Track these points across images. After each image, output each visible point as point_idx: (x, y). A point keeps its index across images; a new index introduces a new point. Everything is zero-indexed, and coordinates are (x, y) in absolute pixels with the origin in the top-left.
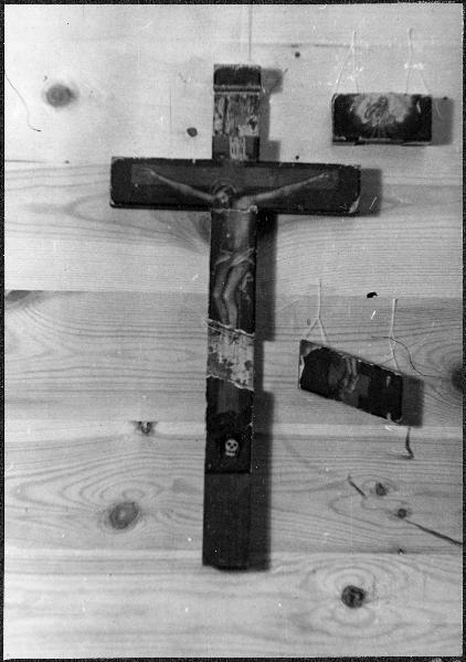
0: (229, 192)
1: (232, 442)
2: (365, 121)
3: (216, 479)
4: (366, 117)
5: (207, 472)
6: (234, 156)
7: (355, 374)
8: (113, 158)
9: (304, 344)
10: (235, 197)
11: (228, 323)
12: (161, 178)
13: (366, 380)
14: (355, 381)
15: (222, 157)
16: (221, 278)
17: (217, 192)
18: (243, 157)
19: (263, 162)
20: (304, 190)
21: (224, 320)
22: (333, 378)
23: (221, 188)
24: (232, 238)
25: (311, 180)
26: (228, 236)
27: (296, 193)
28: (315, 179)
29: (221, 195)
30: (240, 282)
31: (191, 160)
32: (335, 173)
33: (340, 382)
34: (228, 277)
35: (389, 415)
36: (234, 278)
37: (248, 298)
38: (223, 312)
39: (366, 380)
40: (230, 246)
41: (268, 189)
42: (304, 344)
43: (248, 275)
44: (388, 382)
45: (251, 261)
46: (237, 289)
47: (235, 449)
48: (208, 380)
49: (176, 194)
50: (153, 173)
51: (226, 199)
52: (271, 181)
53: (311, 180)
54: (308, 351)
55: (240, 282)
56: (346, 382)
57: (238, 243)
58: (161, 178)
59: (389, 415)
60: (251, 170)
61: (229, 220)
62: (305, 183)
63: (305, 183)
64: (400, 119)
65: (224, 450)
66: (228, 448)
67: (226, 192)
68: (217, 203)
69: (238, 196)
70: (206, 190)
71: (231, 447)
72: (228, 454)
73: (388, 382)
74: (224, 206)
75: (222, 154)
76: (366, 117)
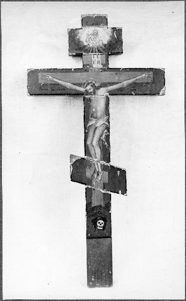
0: (93, 86)
1: (101, 221)
2: (85, 44)
3: (93, 241)
4: (86, 41)
5: (88, 238)
6: (94, 66)
7: (100, 171)
8: (28, 70)
9: (72, 156)
10: (96, 88)
11: (96, 158)
12: (55, 80)
13: (106, 173)
14: (100, 175)
15: (88, 67)
16: (91, 134)
17: (86, 86)
18: (101, 66)
19: (111, 69)
20: (135, 83)
21: (93, 156)
22: (89, 173)
23: (88, 84)
24: (96, 112)
25: (138, 78)
26: (94, 110)
27: (130, 85)
28: (140, 76)
29: (89, 87)
30: (101, 135)
31: (71, 69)
32: (151, 73)
33: (93, 176)
34: (94, 132)
35: (120, 192)
36: (98, 133)
37: (106, 144)
38: (92, 152)
39: (106, 173)
40: (95, 115)
41: (113, 84)
42: (72, 156)
43: (106, 131)
44: (118, 174)
45: (107, 124)
46: (100, 140)
47: (102, 225)
48: (86, 188)
49: (64, 88)
50: (50, 77)
51: (92, 90)
52: (116, 79)
53: (138, 78)
54: (74, 160)
55: (101, 135)
56: (95, 175)
57: (99, 114)
58: (55, 80)
59: (120, 192)
60: (104, 73)
61: (93, 102)
62: (135, 79)
63: (135, 79)
64: (105, 42)
65: (96, 226)
66: (98, 225)
67: (91, 86)
68: (87, 93)
69: (98, 88)
70: (80, 85)
71: (100, 223)
72: (98, 228)
73: (118, 174)
74: (90, 94)
75: (88, 65)
76: (86, 41)
